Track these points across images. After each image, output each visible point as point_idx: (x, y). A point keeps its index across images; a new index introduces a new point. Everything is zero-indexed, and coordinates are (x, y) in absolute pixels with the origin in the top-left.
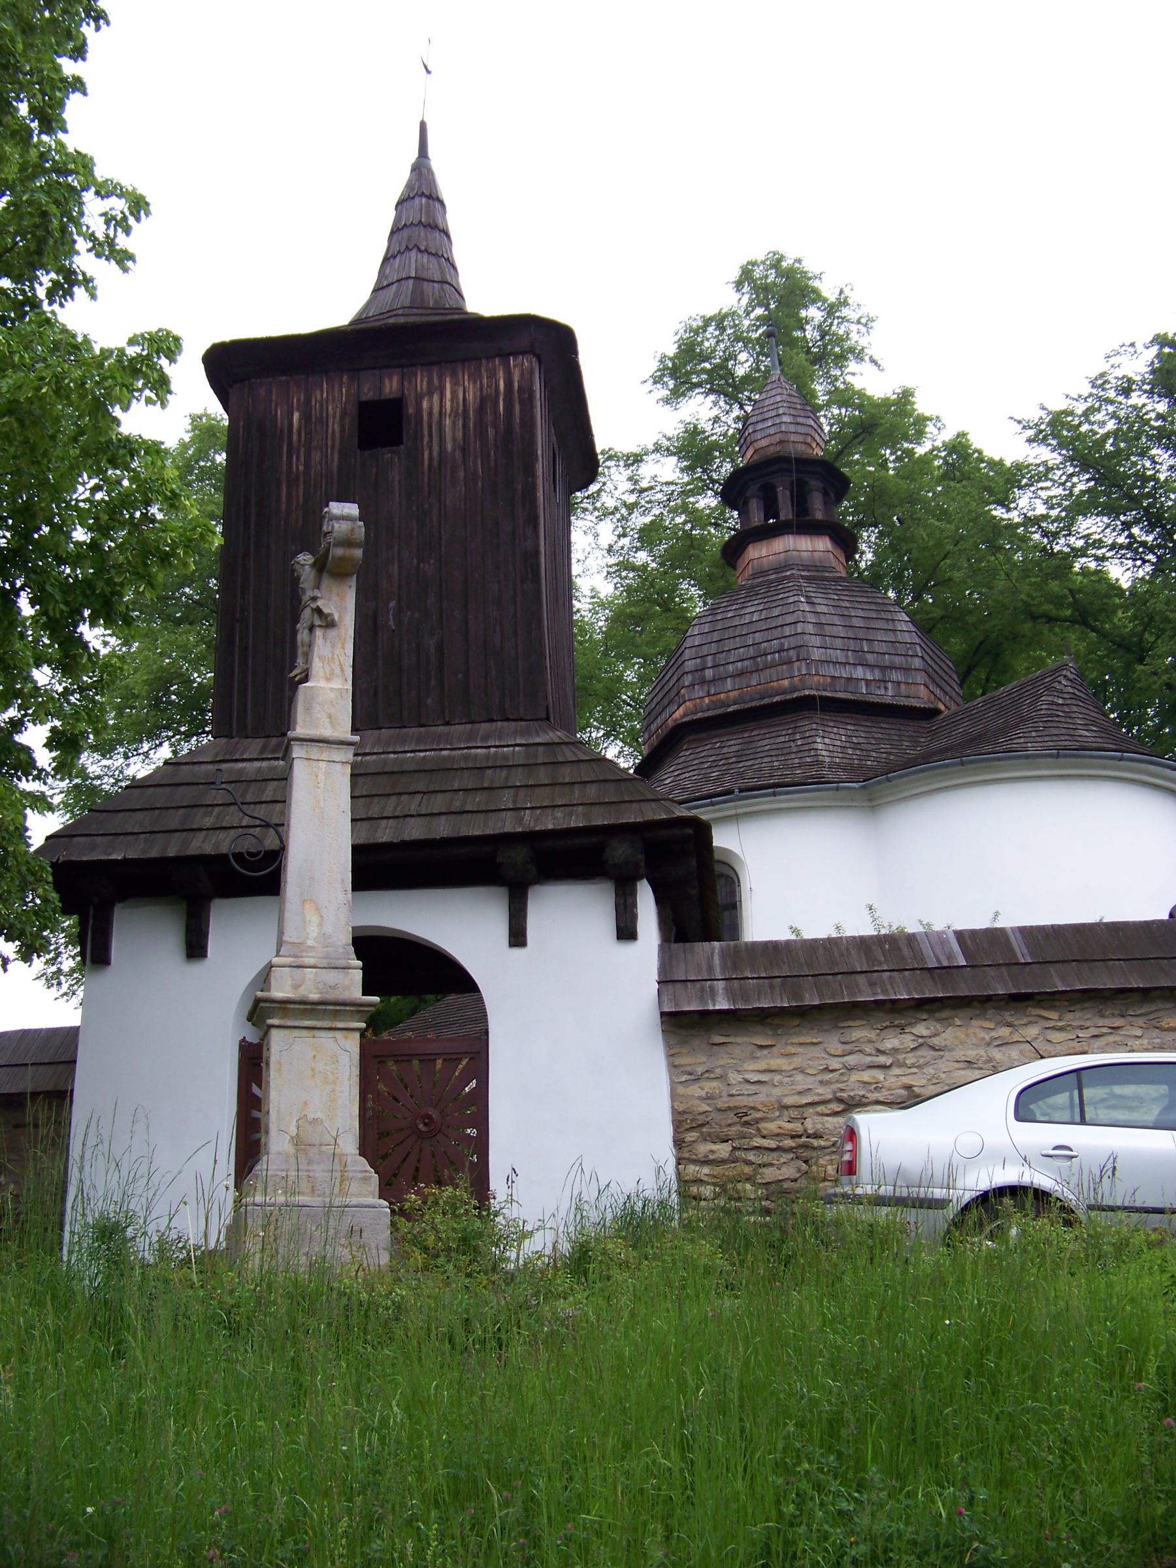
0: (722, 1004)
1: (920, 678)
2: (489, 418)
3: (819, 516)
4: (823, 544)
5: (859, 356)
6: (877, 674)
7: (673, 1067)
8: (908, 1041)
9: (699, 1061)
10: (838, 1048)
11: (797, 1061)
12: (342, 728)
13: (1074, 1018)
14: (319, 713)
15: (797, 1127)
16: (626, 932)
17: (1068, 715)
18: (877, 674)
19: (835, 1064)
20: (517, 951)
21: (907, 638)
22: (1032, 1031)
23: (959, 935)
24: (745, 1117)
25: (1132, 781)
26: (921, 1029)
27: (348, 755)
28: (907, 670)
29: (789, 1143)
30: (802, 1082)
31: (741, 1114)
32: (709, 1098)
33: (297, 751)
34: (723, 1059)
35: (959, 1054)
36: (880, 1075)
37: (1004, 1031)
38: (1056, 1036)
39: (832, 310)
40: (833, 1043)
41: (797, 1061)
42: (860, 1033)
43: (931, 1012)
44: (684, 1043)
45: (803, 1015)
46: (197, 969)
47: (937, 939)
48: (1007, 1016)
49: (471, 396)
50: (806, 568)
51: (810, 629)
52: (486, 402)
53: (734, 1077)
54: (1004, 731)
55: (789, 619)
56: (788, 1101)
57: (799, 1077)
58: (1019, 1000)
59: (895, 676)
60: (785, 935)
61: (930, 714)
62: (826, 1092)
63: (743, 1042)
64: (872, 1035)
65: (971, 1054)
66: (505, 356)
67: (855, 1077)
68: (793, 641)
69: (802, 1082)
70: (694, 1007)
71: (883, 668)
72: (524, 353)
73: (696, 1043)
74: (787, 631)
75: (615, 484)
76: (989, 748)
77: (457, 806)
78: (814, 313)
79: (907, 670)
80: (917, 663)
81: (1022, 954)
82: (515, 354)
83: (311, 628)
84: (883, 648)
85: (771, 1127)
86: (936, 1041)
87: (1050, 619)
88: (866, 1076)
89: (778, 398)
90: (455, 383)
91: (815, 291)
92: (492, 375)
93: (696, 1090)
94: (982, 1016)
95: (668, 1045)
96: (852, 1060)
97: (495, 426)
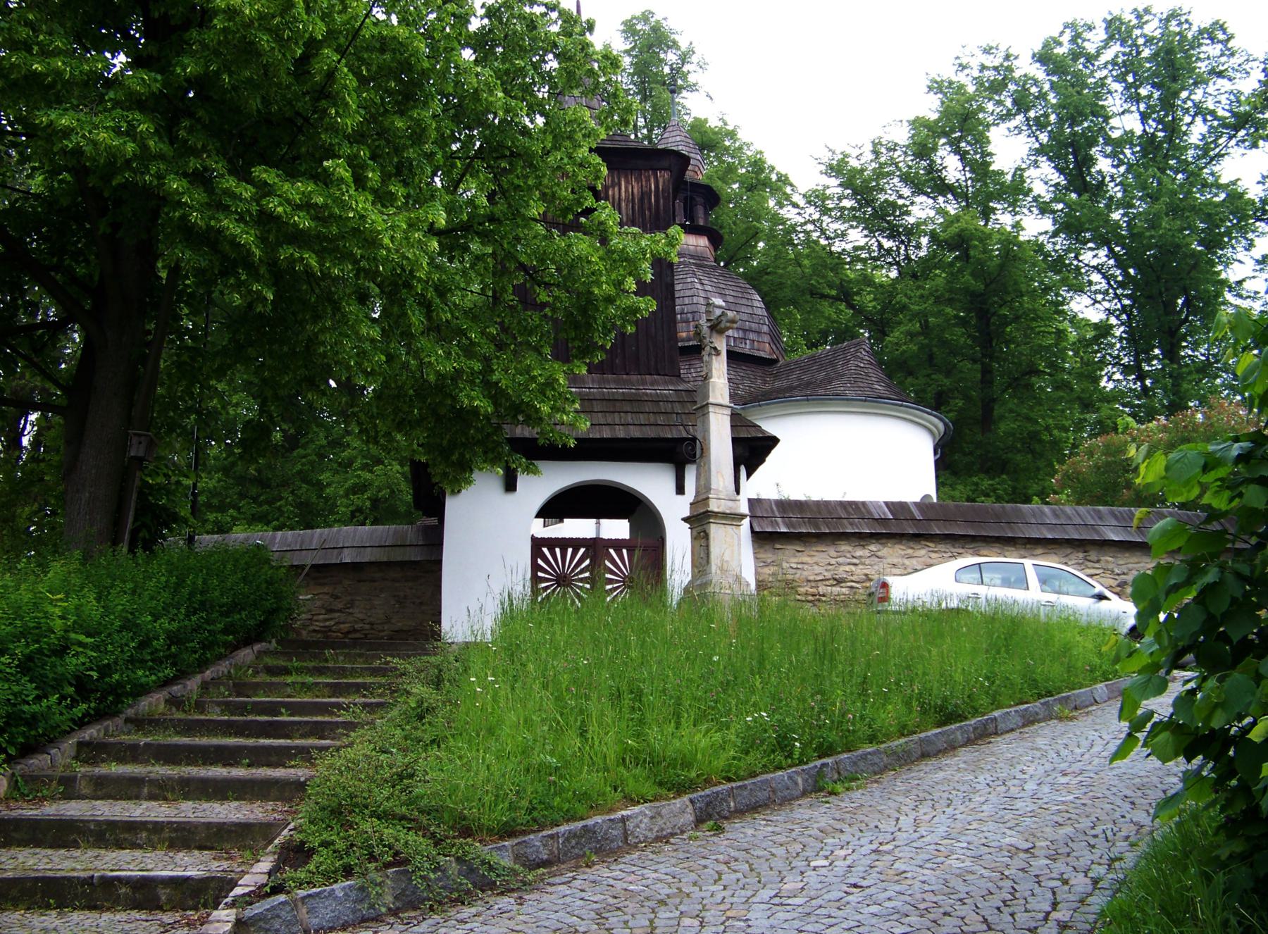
0: (784, 529)
1: (767, 339)
2: (646, 206)
3: (701, 223)
4: (703, 242)
5: (692, 88)
6: (741, 334)
7: (756, 558)
8: (866, 553)
9: (769, 556)
10: (833, 553)
11: (815, 559)
12: (726, 400)
13: (941, 547)
14: (718, 393)
15: (814, 590)
16: (680, 490)
17: (867, 374)
18: (741, 334)
19: (833, 561)
20: (680, 497)
21: (760, 312)
22: (923, 552)
23: (886, 503)
24: (790, 585)
25: (911, 421)
26: (873, 547)
27: (729, 412)
28: (759, 333)
29: (810, 598)
30: (817, 569)
31: (787, 583)
32: (773, 574)
33: (711, 409)
34: (780, 555)
35: (890, 560)
36: (853, 568)
37: (910, 551)
38: (933, 555)
39: (684, 58)
40: (832, 551)
41: (815, 559)
42: (845, 547)
43: (877, 540)
44: (761, 547)
45: (819, 538)
46: (511, 497)
47: (876, 504)
48: (911, 544)
49: (635, 190)
50: (692, 257)
51: (702, 301)
52: (644, 195)
53: (785, 565)
54: (829, 380)
55: (688, 293)
56: (811, 578)
57: (816, 567)
58: (917, 537)
59: (752, 336)
60: (803, 498)
61: (771, 362)
62: (828, 575)
63: (790, 548)
64: (850, 548)
65: (895, 561)
66: (655, 170)
67: (842, 568)
68: (690, 308)
69: (817, 569)
70: (769, 530)
71: (745, 331)
72: (665, 169)
73: (767, 547)
74: (687, 301)
75: (683, 236)
76: (822, 392)
77: (652, 421)
78: (671, 57)
79: (759, 333)
80: (765, 329)
81: (918, 516)
82: (661, 170)
83: (710, 354)
84: (745, 317)
85: (802, 590)
86: (879, 554)
87: (823, 296)
88: (847, 568)
89: (678, 138)
90: (627, 182)
91: (675, 42)
92: (648, 180)
93: (767, 571)
94: (900, 543)
95: (754, 548)
96: (841, 560)
97: (650, 209)
